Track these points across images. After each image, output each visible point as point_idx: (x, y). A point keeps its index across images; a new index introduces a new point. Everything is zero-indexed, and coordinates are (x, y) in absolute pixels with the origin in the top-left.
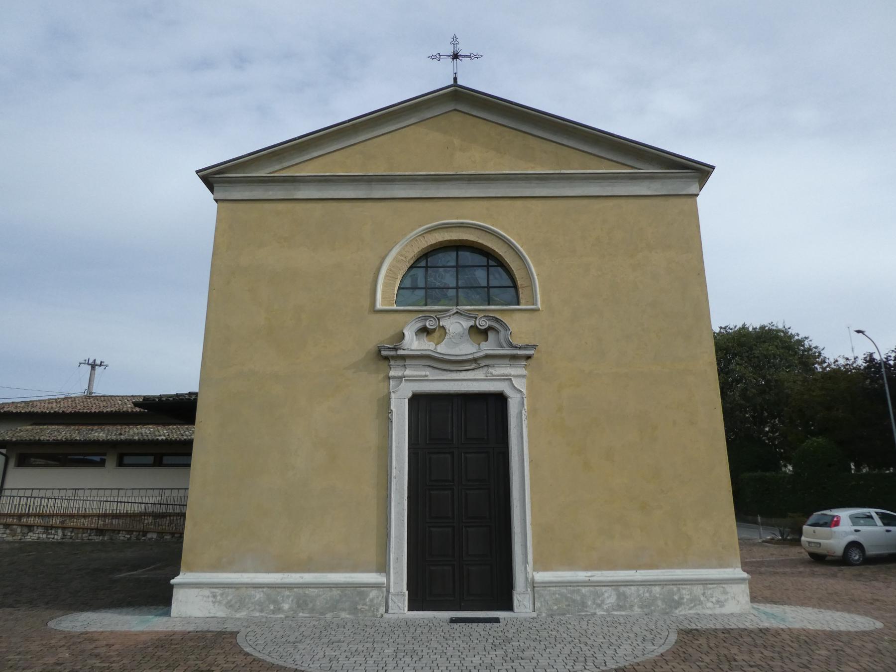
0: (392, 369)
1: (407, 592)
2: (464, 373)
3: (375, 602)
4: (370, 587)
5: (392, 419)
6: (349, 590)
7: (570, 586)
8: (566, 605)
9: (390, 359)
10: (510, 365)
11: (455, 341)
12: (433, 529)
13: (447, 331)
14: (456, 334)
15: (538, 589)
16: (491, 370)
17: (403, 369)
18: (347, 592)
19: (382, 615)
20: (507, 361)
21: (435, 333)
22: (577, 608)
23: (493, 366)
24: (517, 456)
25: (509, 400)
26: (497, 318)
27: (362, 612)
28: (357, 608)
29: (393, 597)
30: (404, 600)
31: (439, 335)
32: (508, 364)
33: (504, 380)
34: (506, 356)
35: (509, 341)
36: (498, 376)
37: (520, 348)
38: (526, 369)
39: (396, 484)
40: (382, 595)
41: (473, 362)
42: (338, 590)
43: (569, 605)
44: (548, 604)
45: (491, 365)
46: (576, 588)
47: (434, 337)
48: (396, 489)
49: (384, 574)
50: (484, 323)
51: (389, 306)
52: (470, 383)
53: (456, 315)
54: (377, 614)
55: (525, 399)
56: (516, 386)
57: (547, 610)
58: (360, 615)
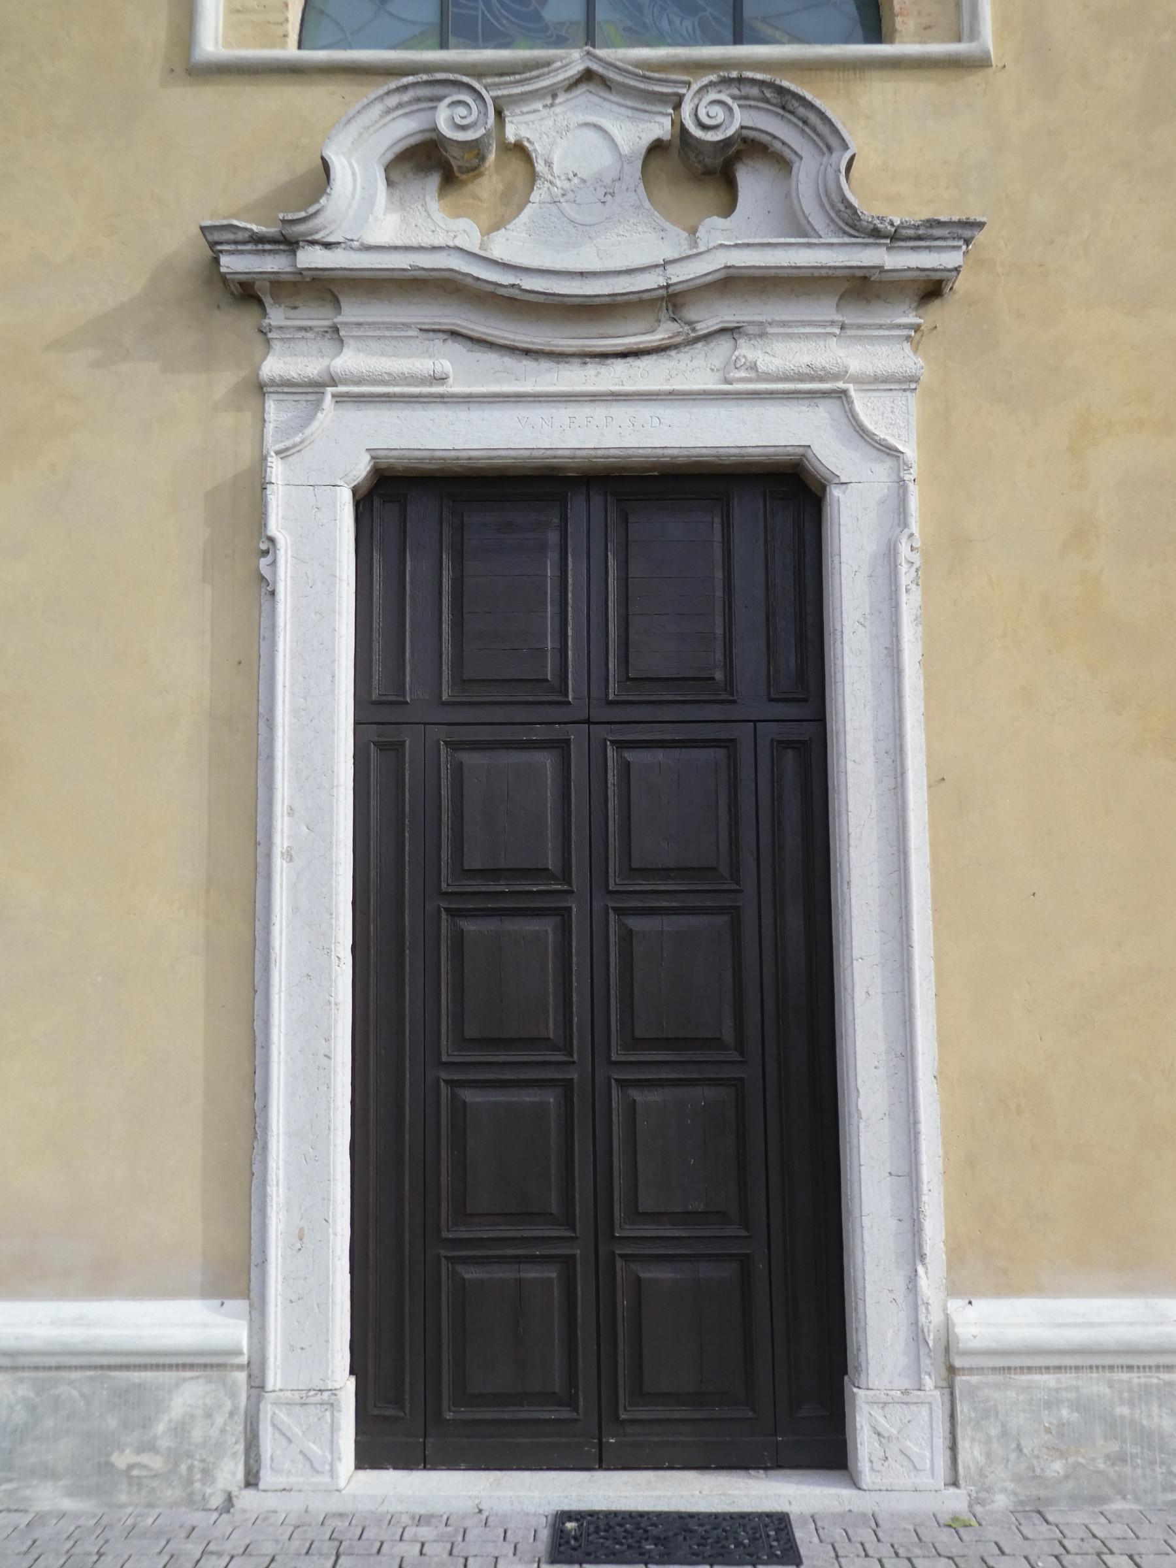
0: (277, 345)
1: (351, 1384)
2: (619, 367)
3: (197, 1435)
4: (170, 1367)
5: (275, 582)
6: (70, 1383)
7: (1130, 1368)
8: (1108, 1457)
9: (268, 301)
10: (843, 327)
11: (579, 218)
12: (470, 1096)
13: (540, 167)
14: (583, 181)
15: (974, 1379)
16: (748, 351)
17: (327, 345)
18: (63, 1390)
19: (229, 1499)
20: (825, 310)
21: (484, 181)
22: (1159, 1470)
23: (761, 333)
24: (870, 760)
25: (835, 492)
26: (781, 91)
27: (136, 1483)
28: (109, 1465)
29: (282, 1415)
30: (334, 1428)
31: (501, 187)
32: (833, 323)
33: (812, 395)
34: (827, 278)
35: (844, 200)
36: (787, 379)
37: (895, 237)
38: (916, 350)
39: (293, 887)
40: (228, 1405)
41: (664, 315)
42: (21, 1380)
43: (1119, 1459)
44: (1019, 1448)
45: (751, 330)
46: (1154, 1379)
47: (476, 197)
48: (295, 910)
49: (241, 1305)
50: (719, 114)
51: (263, 46)
52: (644, 412)
53: (582, 89)
54: (208, 1491)
55: (913, 489)
56: (869, 425)
57: (1018, 1478)
58: (123, 1498)
